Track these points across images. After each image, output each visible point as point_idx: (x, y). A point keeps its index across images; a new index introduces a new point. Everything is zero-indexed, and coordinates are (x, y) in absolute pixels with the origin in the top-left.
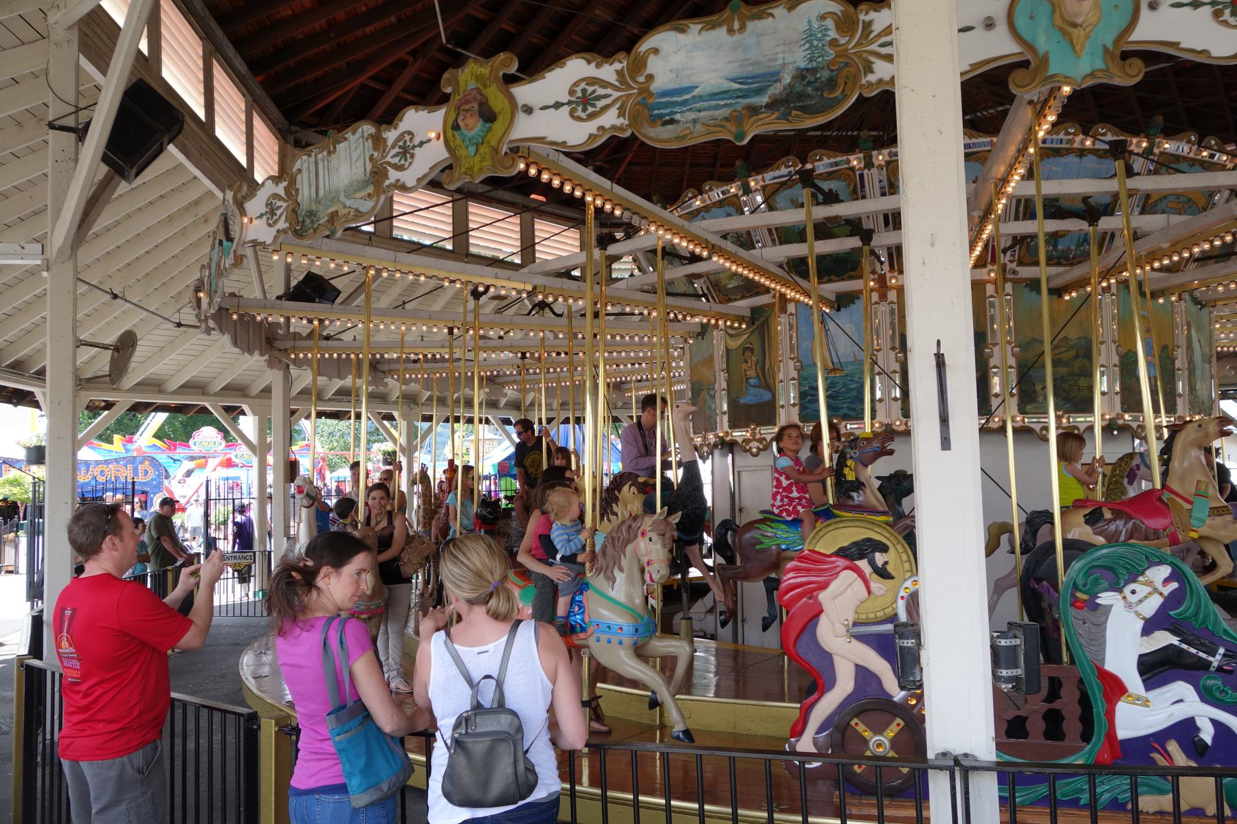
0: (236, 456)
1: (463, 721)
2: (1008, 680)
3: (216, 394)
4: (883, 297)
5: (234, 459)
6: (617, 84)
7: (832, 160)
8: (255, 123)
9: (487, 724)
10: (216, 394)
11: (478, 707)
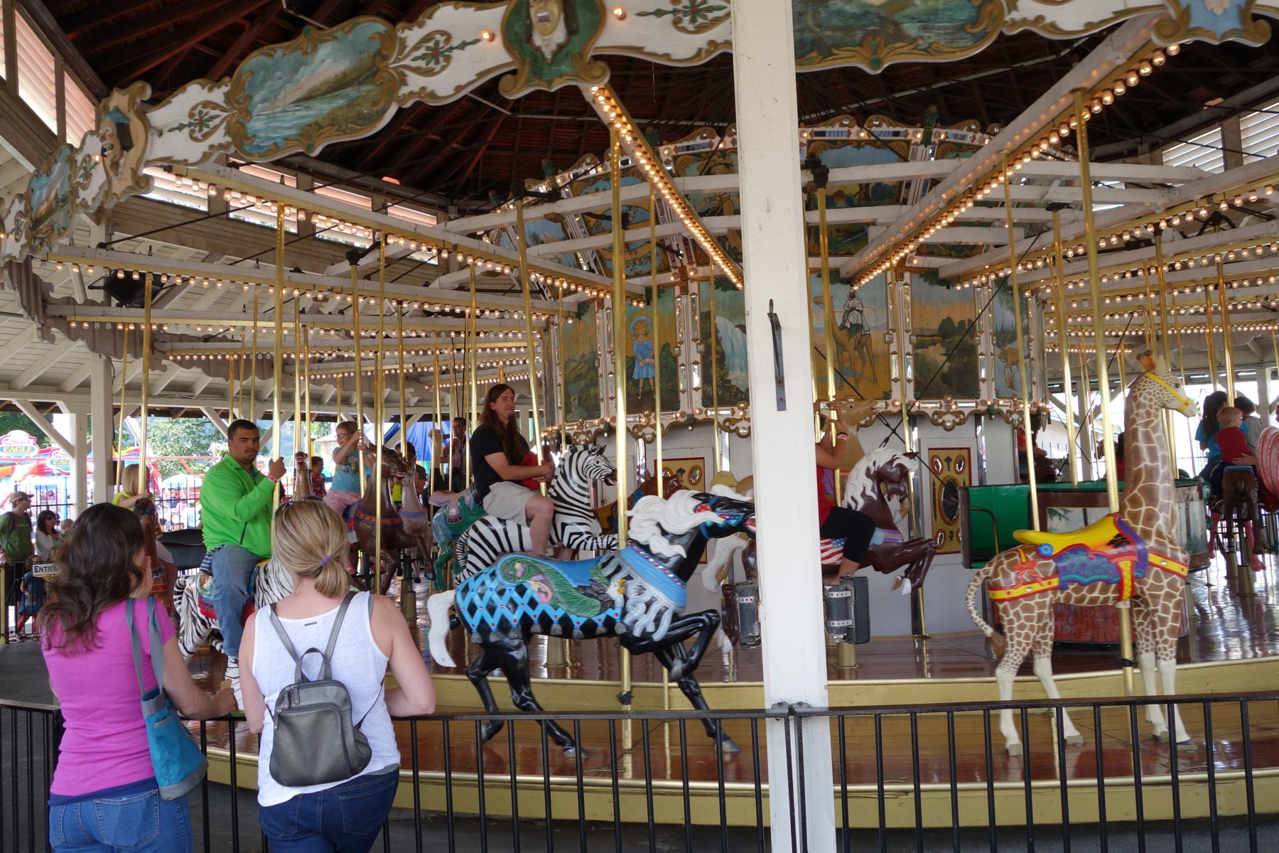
0: (52, 463)
1: (287, 695)
2: (840, 630)
3: (25, 389)
4: (685, 291)
5: (49, 465)
6: (407, 72)
7: (892, 129)
8: (67, 85)
9: (308, 698)
10: (25, 389)
11: (303, 681)
